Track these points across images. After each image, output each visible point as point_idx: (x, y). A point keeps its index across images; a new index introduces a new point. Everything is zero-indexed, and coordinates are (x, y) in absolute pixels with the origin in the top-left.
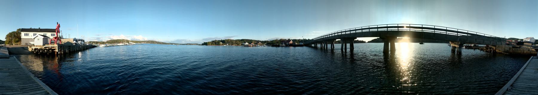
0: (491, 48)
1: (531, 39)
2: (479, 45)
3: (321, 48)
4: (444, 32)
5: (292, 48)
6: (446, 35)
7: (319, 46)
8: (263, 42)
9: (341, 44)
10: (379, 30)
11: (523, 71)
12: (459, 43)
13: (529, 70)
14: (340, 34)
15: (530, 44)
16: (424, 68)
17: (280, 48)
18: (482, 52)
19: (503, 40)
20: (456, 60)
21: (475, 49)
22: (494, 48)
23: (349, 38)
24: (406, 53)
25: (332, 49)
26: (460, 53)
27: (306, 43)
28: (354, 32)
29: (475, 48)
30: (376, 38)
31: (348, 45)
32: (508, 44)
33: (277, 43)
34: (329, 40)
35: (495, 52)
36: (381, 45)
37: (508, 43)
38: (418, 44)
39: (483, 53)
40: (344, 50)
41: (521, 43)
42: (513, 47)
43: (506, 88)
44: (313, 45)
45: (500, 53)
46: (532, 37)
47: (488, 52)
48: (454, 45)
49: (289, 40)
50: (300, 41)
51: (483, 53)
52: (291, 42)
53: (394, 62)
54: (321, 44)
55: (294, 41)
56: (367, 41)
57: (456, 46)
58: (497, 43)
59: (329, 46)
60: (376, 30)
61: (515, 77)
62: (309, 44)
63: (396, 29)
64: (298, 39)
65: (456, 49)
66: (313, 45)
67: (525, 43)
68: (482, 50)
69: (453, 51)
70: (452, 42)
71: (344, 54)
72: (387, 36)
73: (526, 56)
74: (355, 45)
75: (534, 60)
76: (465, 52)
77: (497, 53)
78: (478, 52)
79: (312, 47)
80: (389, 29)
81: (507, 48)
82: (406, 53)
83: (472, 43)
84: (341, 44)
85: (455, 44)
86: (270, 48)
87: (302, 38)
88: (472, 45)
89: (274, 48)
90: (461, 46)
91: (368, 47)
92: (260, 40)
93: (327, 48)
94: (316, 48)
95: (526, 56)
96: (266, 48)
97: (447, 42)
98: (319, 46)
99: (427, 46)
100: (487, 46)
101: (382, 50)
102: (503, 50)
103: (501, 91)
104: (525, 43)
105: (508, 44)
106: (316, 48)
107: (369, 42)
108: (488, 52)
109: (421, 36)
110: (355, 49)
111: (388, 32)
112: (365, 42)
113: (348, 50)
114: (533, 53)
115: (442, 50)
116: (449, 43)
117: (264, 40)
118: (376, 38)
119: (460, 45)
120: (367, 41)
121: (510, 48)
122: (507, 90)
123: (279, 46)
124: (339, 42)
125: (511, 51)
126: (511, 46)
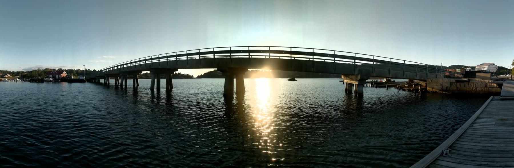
0: (416, 85)
1: (490, 65)
2: (397, 80)
3: (116, 86)
4: (330, 60)
5: (65, 85)
6: (335, 65)
7: (112, 82)
8: (15, 74)
9: (150, 81)
10: (217, 55)
11: (474, 122)
12: (359, 78)
13: (485, 120)
14: (150, 62)
15: (489, 75)
16: (298, 123)
17: (44, 85)
18: (401, 92)
19: (441, 69)
20: (355, 106)
21: (388, 87)
22: (423, 84)
23: (165, 70)
24: (266, 98)
25: (135, 89)
26: (360, 95)
27: (91, 77)
28: (174, 59)
29: (388, 85)
30: (212, 70)
31: (163, 82)
32: (449, 77)
33: (40, 75)
34: (131, 72)
35: (424, 92)
36: (220, 83)
37: (448, 74)
38: (285, 81)
39: (403, 93)
40: (155, 90)
41: (470, 73)
42: (457, 81)
43: (440, 151)
44: (102, 81)
45: (433, 93)
46: (491, 62)
47: (412, 91)
48: (349, 81)
49: (60, 71)
50: (79, 73)
51: (403, 93)
52: (64, 74)
53: (243, 112)
54: (116, 79)
55: (70, 72)
56: (195, 76)
57: (353, 82)
58: (429, 75)
59: (130, 82)
60: (211, 56)
61: (459, 132)
62: (95, 79)
63: (245, 55)
64: (76, 68)
65: (354, 89)
66: (102, 81)
67: (478, 74)
68: (401, 88)
69: (348, 91)
70: (347, 76)
71: (155, 97)
72: (231, 67)
73: (481, 97)
74: (175, 81)
75: (494, 103)
76: (370, 93)
77: (428, 92)
78: (393, 91)
79: (101, 84)
80: (234, 55)
81: (446, 83)
82: (266, 98)
83: (383, 78)
84: (150, 81)
85: (352, 79)
86: (27, 85)
87: (82, 68)
88: (384, 80)
89: (35, 85)
90: (362, 83)
91: (198, 86)
92: (9, 70)
93: (126, 85)
94: (106, 85)
95: (481, 97)
96: (18, 84)
97: (338, 76)
98: (112, 82)
99: (307, 84)
100: (411, 81)
101: (222, 89)
102: (440, 87)
103: (429, 158)
104: (478, 74)
105: (449, 77)
106: (106, 85)
107: (199, 77)
108: (412, 91)
109: (294, 67)
110: (175, 91)
111: (231, 59)
112: (192, 77)
113: (163, 91)
114: (495, 90)
115: (329, 90)
116: (340, 78)
117: (16, 70)
118: (212, 70)
119: (359, 81)
120: (195, 76)
121: (451, 84)
122: (442, 154)
123: (42, 81)
124: (146, 76)
125: (454, 88)
126: (453, 80)
